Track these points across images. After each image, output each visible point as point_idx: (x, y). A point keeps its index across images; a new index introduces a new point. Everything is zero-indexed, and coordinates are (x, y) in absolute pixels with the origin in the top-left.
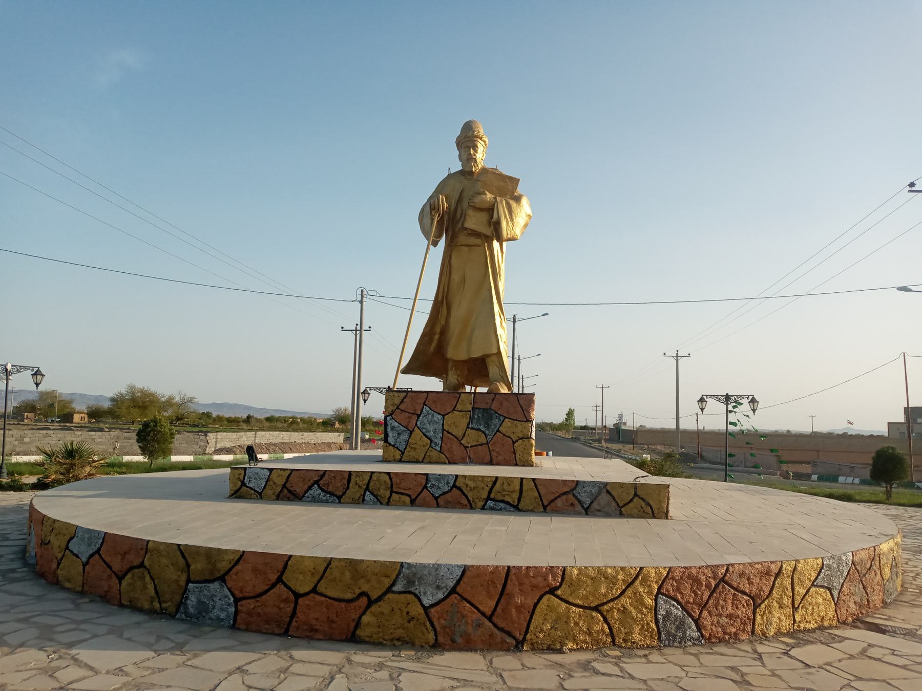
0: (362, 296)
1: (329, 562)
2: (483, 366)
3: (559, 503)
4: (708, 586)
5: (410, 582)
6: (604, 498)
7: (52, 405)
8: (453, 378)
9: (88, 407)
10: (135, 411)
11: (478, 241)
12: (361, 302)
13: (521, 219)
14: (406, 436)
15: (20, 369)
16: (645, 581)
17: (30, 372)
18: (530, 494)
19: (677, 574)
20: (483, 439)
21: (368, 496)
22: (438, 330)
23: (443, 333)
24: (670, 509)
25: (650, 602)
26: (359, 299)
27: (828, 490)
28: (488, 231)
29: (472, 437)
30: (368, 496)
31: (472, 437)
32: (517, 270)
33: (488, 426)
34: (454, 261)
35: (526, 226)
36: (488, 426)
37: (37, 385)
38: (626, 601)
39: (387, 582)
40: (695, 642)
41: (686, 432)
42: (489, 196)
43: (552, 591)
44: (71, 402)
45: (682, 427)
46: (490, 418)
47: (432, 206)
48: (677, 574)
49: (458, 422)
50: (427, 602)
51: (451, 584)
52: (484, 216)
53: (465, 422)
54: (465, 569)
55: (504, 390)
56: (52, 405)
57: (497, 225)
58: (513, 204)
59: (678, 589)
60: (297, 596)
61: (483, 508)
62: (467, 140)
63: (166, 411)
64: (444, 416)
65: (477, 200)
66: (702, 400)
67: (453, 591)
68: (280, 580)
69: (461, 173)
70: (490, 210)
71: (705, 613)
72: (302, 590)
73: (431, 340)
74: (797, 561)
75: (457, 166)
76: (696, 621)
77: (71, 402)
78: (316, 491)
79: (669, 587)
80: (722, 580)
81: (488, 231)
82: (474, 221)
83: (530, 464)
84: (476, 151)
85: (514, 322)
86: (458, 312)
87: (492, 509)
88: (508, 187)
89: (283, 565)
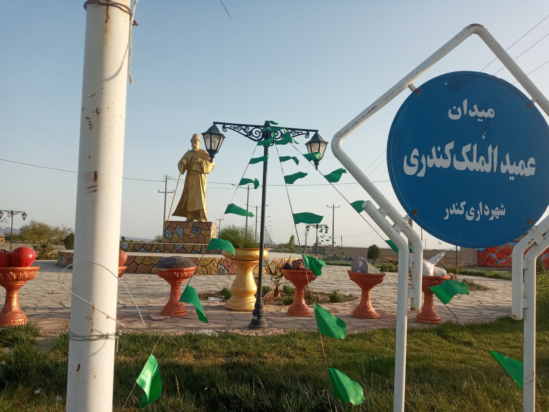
0: (166, 179)
2: (199, 213)
8: (189, 217)
9: (5, 234)
10: (35, 236)
11: (197, 173)
12: (166, 181)
15: (17, 212)
16: (215, 261)
18: (204, 249)
21: (158, 250)
22: (184, 201)
23: (186, 202)
25: (216, 265)
26: (165, 180)
27: (341, 263)
28: (200, 170)
29: (192, 235)
30: (158, 250)
31: (192, 235)
34: (190, 180)
35: (213, 169)
36: (197, 232)
38: (211, 265)
40: (227, 274)
42: (200, 160)
47: (181, 163)
49: (188, 231)
52: (199, 166)
55: (204, 221)
57: (202, 169)
60: (138, 264)
63: (54, 236)
65: (196, 161)
68: (134, 261)
70: (200, 164)
75: (191, 149)
78: (142, 249)
79: (221, 262)
81: (200, 170)
82: (195, 167)
85: (248, 189)
86: (191, 195)
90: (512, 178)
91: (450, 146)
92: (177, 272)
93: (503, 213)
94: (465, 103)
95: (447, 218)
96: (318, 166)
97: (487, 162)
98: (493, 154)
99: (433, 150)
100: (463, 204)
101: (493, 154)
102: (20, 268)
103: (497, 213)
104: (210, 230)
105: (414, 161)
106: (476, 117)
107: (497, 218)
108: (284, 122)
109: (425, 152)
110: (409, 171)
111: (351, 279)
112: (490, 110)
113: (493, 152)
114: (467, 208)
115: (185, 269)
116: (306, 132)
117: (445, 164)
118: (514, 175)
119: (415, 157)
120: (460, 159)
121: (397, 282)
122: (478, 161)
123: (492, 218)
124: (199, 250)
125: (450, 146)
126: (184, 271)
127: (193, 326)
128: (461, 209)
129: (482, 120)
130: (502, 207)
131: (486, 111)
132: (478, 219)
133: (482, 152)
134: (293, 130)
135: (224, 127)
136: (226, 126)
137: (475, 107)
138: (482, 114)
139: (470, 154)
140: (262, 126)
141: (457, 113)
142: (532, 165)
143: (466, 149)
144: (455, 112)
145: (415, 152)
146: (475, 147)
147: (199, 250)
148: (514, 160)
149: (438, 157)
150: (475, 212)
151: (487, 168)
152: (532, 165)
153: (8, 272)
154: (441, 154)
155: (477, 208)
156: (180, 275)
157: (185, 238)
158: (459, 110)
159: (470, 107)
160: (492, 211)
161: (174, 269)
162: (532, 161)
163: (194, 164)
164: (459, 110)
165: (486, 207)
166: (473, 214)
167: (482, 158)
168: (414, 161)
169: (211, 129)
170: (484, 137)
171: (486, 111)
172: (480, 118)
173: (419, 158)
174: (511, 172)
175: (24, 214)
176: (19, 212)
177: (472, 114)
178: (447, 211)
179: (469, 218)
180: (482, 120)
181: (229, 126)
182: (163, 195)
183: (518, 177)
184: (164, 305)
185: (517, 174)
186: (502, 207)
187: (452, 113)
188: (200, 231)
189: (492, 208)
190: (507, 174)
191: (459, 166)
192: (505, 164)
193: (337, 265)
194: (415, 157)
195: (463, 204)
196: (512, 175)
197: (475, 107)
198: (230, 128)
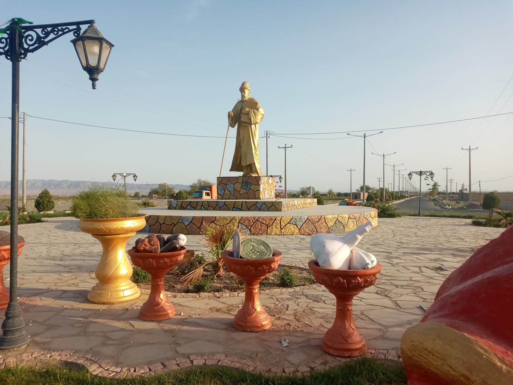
1: (166, 216)
2: (251, 167)
3: (252, 208)
4: (253, 221)
5: (182, 220)
6: (264, 206)
7: (165, 190)
11: (247, 125)
13: (259, 117)
14: (223, 191)
15: (128, 175)
16: (235, 220)
17: (132, 176)
18: (244, 206)
19: (244, 218)
20: (246, 192)
21: (202, 208)
22: (239, 155)
28: (248, 121)
29: (242, 191)
30: (202, 208)
33: (247, 187)
34: (241, 132)
35: (262, 118)
36: (247, 187)
37: (114, 180)
38: (230, 224)
39: (178, 220)
41: (475, 193)
42: (247, 109)
43: (213, 222)
44: (173, 189)
45: (472, 190)
46: (248, 185)
48: (244, 218)
49: (238, 186)
50: (186, 224)
51: (191, 220)
53: (240, 186)
54: (194, 217)
56: (165, 190)
57: (250, 119)
58: (256, 111)
59: (244, 222)
60: (161, 224)
61: (232, 210)
62: (242, 89)
66: (410, 174)
67: (191, 222)
68: (157, 221)
70: (248, 114)
71: (252, 228)
72: (162, 223)
73: (237, 159)
74: (282, 217)
76: (249, 230)
77: (173, 189)
78: (189, 207)
80: (257, 220)
82: (243, 118)
83: (260, 199)
84: (245, 93)
85: (365, 137)
87: (235, 210)
88: (253, 105)
89: (158, 217)
96: (97, 83)
104: (259, 185)
108: (37, 16)
116: (75, 27)
121: (308, 268)
134: (54, 26)
157: (236, 194)
163: (242, 115)
175: (135, 176)
176: (131, 174)
182: (283, 150)
188: (249, 186)
193: (445, 216)
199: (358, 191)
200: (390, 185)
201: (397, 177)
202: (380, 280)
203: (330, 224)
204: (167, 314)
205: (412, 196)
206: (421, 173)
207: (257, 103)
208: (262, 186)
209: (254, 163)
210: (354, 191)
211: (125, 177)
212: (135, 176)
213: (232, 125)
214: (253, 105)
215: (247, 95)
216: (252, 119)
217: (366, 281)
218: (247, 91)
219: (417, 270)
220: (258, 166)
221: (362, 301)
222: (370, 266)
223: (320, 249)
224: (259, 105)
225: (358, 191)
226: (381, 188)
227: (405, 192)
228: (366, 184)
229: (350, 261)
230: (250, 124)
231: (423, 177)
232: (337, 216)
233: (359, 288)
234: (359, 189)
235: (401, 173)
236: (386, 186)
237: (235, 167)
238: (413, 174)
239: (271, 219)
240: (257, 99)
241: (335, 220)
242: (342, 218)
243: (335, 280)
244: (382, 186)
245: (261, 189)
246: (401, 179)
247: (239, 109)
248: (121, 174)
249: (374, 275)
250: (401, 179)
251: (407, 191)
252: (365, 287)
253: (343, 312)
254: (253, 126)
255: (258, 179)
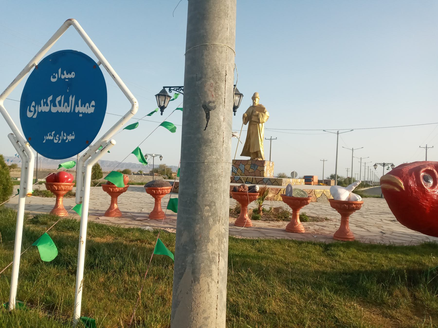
2: (257, 154)
6: (269, 181)
7: (164, 170)
13: (265, 118)
15: (156, 155)
18: (254, 181)
22: (248, 145)
23: (249, 146)
24: (368, 198)
28: (258, 121)
29: (251, 171)
31: (251, 171)
32: (264, 131)
34: (251, 128)
35: (268, 119)
36: (254, 168)
42: (257, 112)
44: (171, 169)
49: (248, 167)
52: (256, 117)
56: (164, 170)
57: (259, 119)
58: (263, 114)
62: (254, 98)
64: (153, 157)
69: (253, 106)
70: (258, 115)
77: (171, 169)
82: (254, 119)
85: (338, 134)
86: (252, 140)
88: (262, 109)
90: (81, 115)
91: (50, 98)
92: (154, 189)
93: (73, 137)
94: (60, 70)
95: (44, 142)
97: (68, 106)
98: (72, 101)
99: (42, 102)
100: (53, 133)
101: (72, 101)
102: (58, 183)
103: (71, 138)
104: (264, 167)
105: (32, 109)
106: (65, 78)
107: (70, 140)
109: (38, 103)
110: (29, 115)
111: (332, 206)
112: (73, 73)
113: (72, 99)
114: (55, 135)
115: (159, 188)
117: (45, 109)
118: (82, 113)
119: (33, 106)
120: (55, 106)
122: (63, 106)
123: (67, 141)
124: (251, 181)
125: (50, 98)
126: (158, 190)
127: (160, 225)
128: (52, 136)
129: (68, 80)
130: (73, 134)
131: (70, 74)
132: (60, 142)
133: (67, 100)
135: (170, 90)
136: (171, 88)
137: (65, 72)
138: (69, 76)
139: (60, 102)
140: (183, 87)
141: (56, 78)
142: (93, 106)
143: (58, 99)
144: (54, 77)
145: (33, 104)
146: (63, 97)
147: (251, 181)
148: (83, 104)
149: (44, 106)
150: (59, 137)
151: (68, 110)
152: (93, 106)
153: (53, 185)
154: (46, 104)
155: (60, 135)
156: (156, 192)
158: (56, 76)
159: (62, 73)
160: (68, 137)
161: (151, 188)
162: (93, 103)
163: (253, 116)
164: (56, 76)
165: (65, 134)
166: (57, 138)
167: (66, 104)
168: (32, 109)
169: (161, 92)
170: (68, 91)
171: (70, 74)
172: (67, 79)
173: (34, 107)
174: (81, 112)
175: (161, 157)
177: (63, 77)
178: (45, 137)
179: (56, 141)
180: (68, 80)
181: (173, 88)
183: (84, 114)
184: (150, 212)
185: (84, 112)
186: (73, 134)
187: (53, 78)
188: (256, 167)
189: (68, 135)
190: (79, 113)
191: (54, 110)
192: (78, 106)
194: (33, 106)
195: (53, 133)
196: (81, 113)
197: (65, 72)
198: (174, 90)
199: (328, 178)
200: (357, 175)
201: (363, 168)
202: (362, 209)
203: (318, 196)
204: (250, 225)
205: (375, 185)
206: (384, 165)
207: (264, 108)
208: (265, 168)
209: (260, 151)
210: (325, 179)
211: (153, 157)
212: (161, 157)
213: (245, 123)
214: (262, 109)
215: (257, 102)
216: (260, 119)
217: (357, 207)
218: (257, 99)
219: (380, 220)
220: (262, 153)
221: (354, 217)
222: (358, 200)
223: (335, 193)
224: (266, 110)
225: (328, 178)
226: (349, 178)
227: (369, 182)
228: (337, 174)
229: (349, 199)
230: (259, 122)
231: (386, 167)
232: (323, 191)
233: (353, 210)
234: (330, 177)
235: (367, 165)
236: (353, 176)
237: (244, 154)
238: (378, 165)
239: (277, 190)
240: (264, 105)
241: (321, 193)
242: (327, 192)
243: (343, 206)
244: (350, 176)
245: (265, 170)
246: (367, 170)
247: (251, 112)
248: (151, 155)
249: (361, 204)
250: (367, 170)
251: (372, 181)
252: (356, 209)
253: (344, 222)
254: (260, 124)
255: (263, 162)
